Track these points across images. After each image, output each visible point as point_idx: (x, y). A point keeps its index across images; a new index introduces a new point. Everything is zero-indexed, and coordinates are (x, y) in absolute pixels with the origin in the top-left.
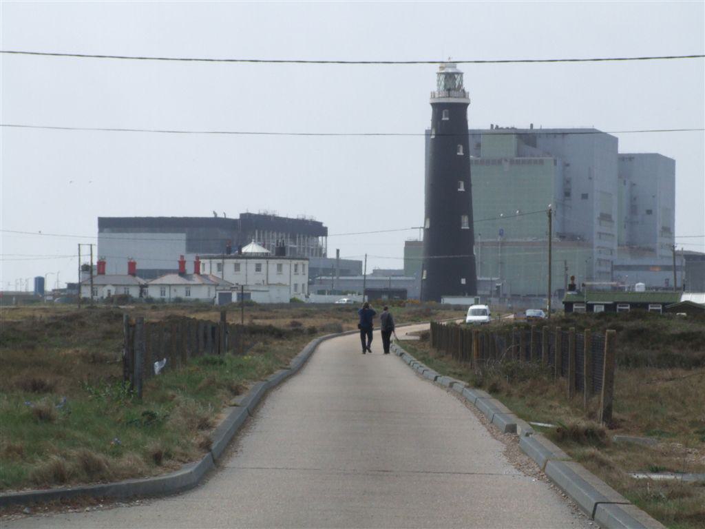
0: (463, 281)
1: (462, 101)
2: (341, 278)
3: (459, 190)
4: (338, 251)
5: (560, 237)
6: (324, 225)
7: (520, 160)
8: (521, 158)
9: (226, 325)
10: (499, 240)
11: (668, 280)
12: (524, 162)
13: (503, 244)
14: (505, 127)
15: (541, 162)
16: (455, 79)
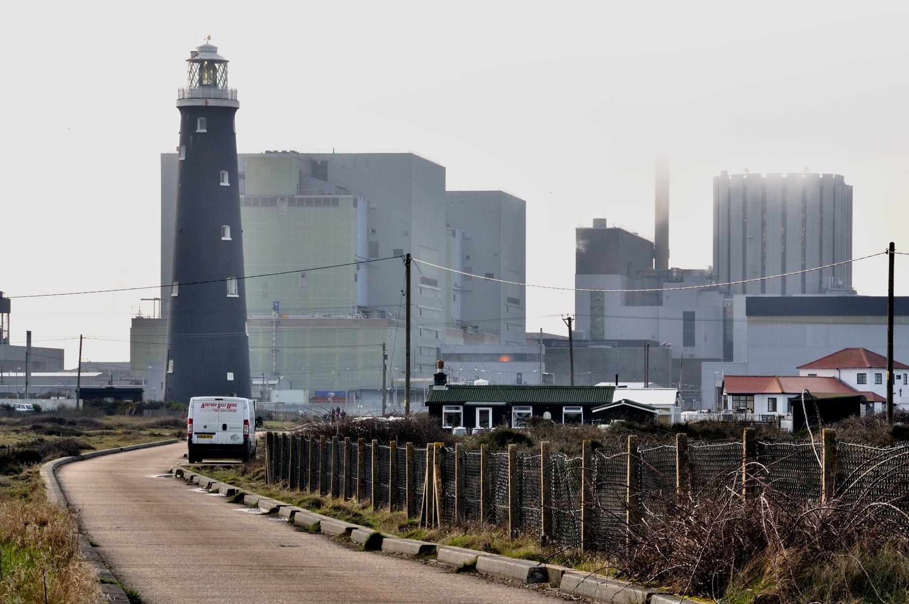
0: (230, 377)
1: (233, 105)
2: (33, 374)
3: (223, 239)
4: (29, 333)
5: (364, 312)
6: (847, 182)
7: (303, 199)
8: (304, 196)
9: (597, 339)
10: (272, 317)
11: (521, 374)
12: (309, 202)
13: (278, 323)
14: (280, 151)
15: (335, 202)
16: (215, 71)
